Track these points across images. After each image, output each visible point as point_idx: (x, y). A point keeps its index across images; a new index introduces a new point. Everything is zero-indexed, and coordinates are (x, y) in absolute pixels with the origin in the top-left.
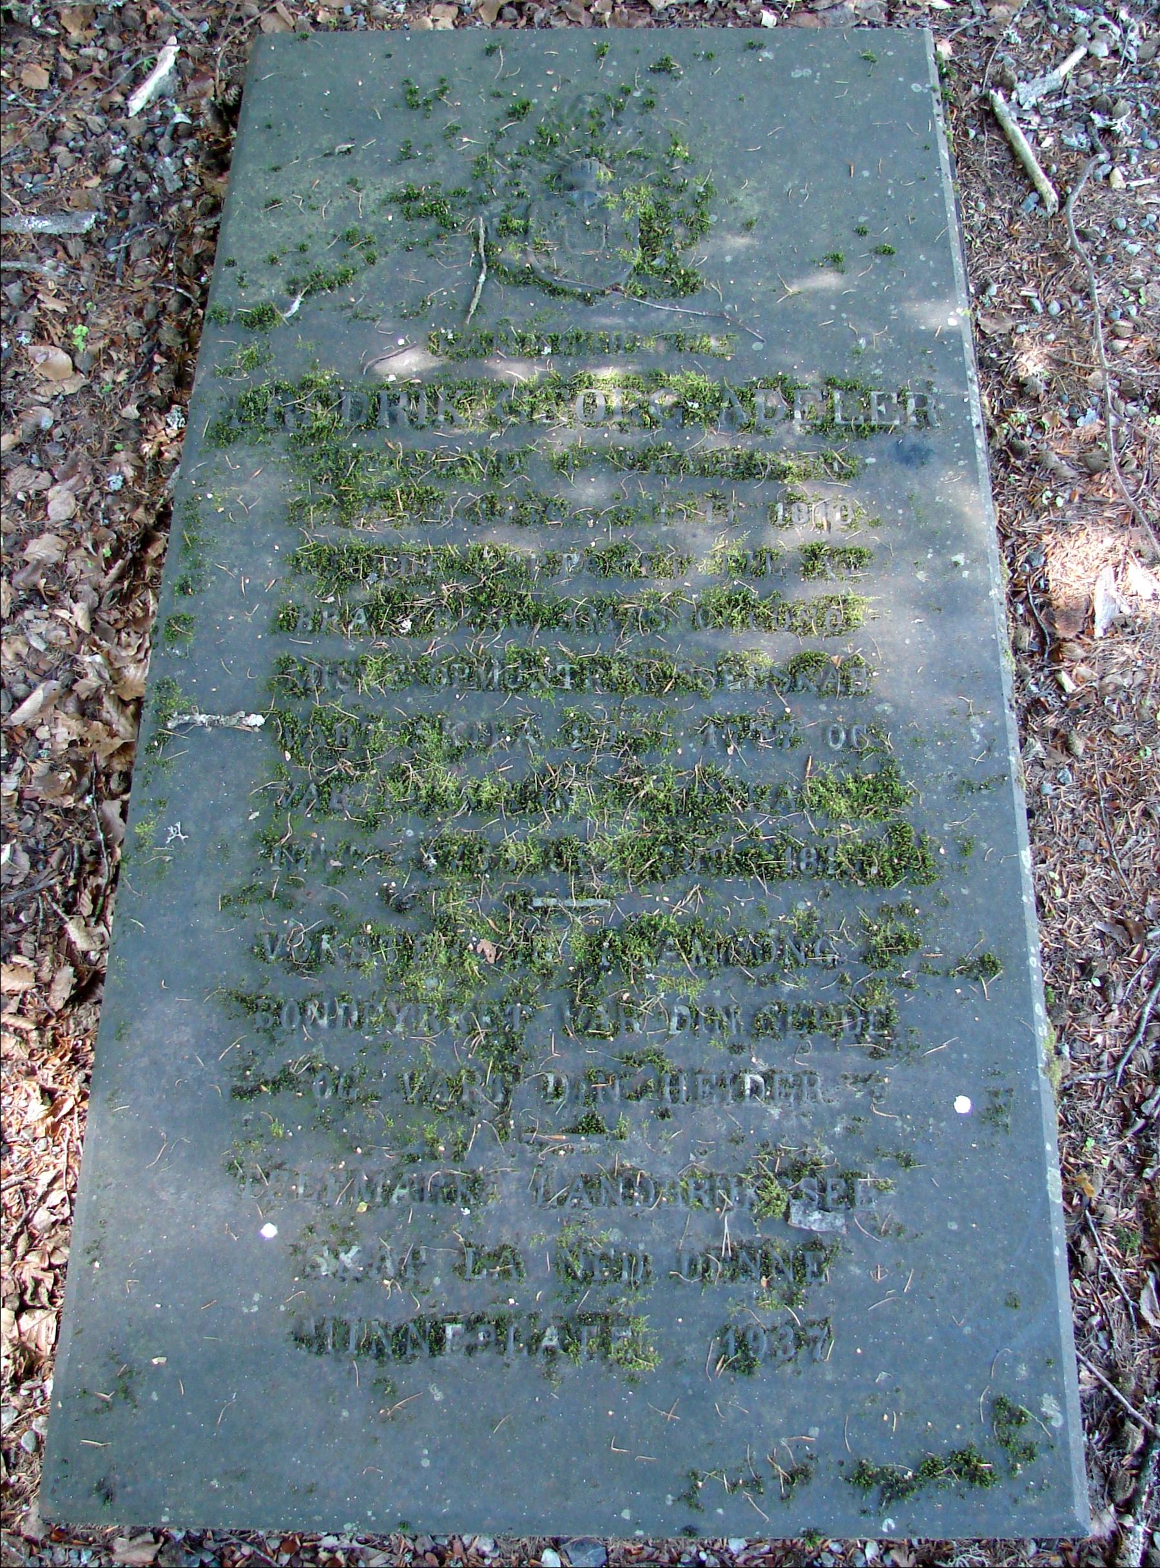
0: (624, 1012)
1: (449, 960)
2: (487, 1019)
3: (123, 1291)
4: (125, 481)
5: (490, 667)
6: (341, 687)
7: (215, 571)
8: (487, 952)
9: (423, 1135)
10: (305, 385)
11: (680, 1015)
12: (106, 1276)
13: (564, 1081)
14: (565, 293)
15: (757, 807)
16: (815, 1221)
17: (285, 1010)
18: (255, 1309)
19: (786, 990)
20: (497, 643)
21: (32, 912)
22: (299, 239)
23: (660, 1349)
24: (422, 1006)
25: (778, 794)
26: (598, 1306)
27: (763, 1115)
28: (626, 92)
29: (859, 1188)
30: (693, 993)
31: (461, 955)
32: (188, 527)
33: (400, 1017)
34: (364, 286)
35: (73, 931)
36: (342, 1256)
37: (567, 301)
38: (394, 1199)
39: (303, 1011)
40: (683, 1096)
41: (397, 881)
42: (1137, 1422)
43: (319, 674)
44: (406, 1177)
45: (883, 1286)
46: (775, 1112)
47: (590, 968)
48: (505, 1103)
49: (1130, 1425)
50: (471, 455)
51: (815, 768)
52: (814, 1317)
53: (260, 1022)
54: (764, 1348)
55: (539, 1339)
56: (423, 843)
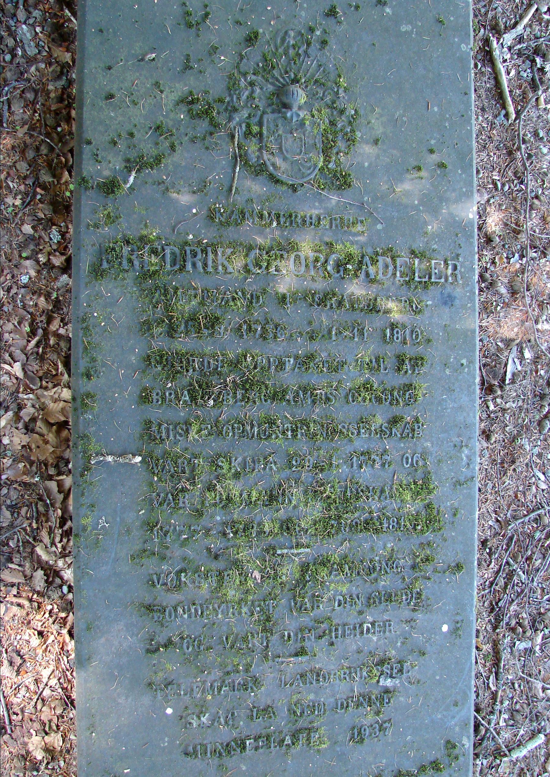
0: (316, 599)
1: (240, 582)
2: (258, 609)
3: (108, 744)
4: (30, 278)
5: (252, 426)
6: (179, 438)
7: (104, 365)
8: (257, 577)
9: (232, 663)
10: (143, 239)
11: (339, 601)
12: (99, 738)
13: (292, 634)
14: (282, 183)
15: (373, 499)
16: (388, 683)
17: (167, 611)
18: (166, 744)
19: (381, 585)
20: (255, 412)
21: (16, 540)
22: (128, 127)
23: (329, 739)
24: (229, 605)
25: (382, 491)
26: (305, 725)
27: (370, 640)
28: (311, 30)
29: (405, 667)
30: (344, 590)
31: (246, 580)
32: (85, 335)
33: (220, 611)
34: (171, 167)
35: (39, 550)
36: (202, 718)
37: (285, 188)
38: (222, 692)
39: (176, 610)
40: (340, 636)
41: (216, 544)
42: (482, 725)
43: (168, 430)
44: (227, 682)
45: (412, 704)
46: (375, 638)
47: (301, 582)
48: (267, 646)
49: (481, 727)
50: (237, 294)
51: (398, 477)
52: (386, 719)
53: (156, 619)
54: (367, 733)
55: (283, 741)
56: (225, 524)
